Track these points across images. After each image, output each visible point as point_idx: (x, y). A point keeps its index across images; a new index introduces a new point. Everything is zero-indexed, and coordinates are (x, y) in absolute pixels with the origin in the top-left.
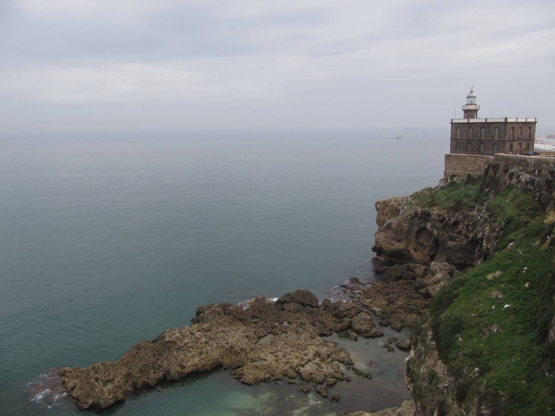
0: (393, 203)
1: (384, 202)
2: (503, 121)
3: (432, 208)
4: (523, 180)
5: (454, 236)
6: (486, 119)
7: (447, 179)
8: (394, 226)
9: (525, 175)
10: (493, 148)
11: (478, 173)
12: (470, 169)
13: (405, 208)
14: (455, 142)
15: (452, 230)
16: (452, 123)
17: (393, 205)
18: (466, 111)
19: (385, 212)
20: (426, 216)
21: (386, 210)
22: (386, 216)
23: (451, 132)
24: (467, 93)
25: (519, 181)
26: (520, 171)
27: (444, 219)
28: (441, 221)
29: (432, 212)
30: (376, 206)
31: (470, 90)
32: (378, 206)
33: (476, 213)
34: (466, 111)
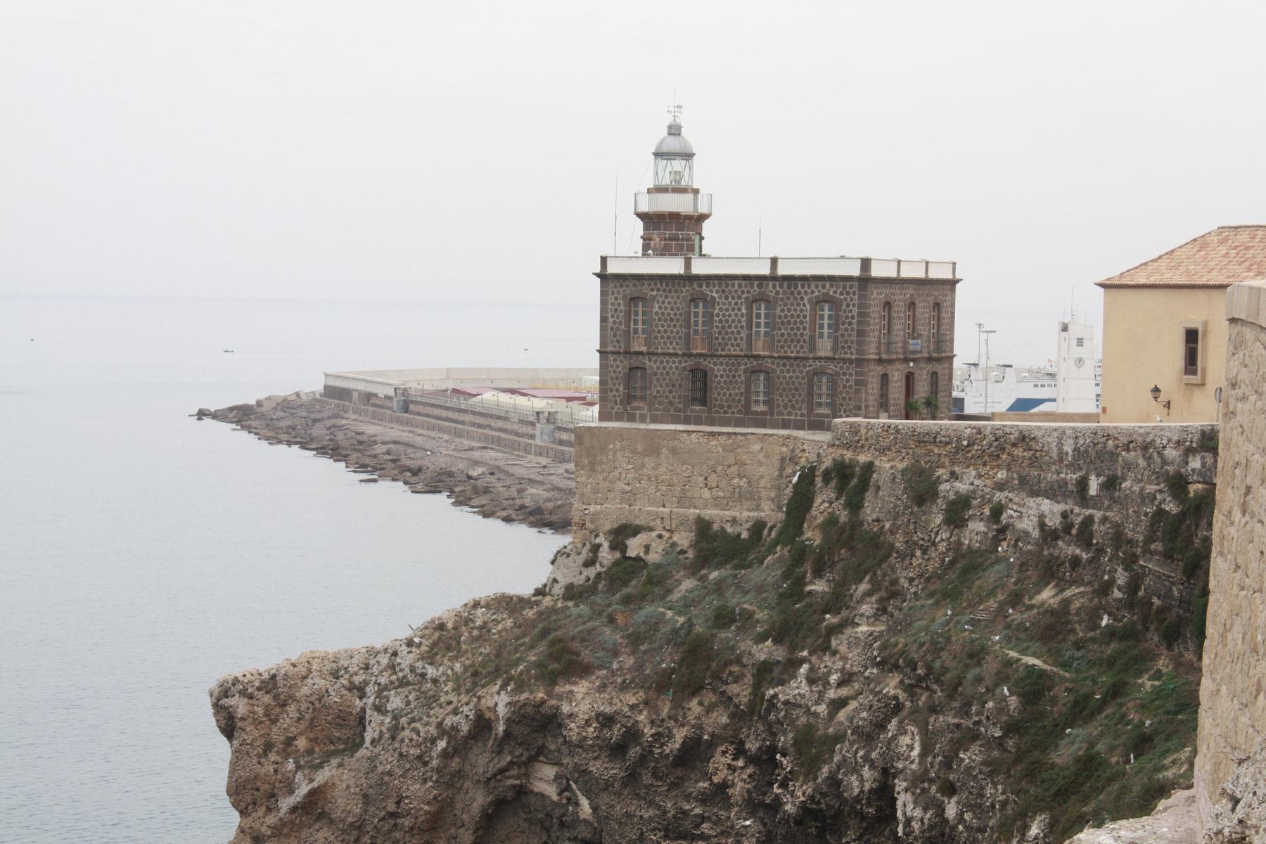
0: (321, 683)
1: (270, 683)
2: (855, 271)
3: (561, 689)
4: (1028, 524)
5: (685, 813)
6: (774, 261)
7: (596, 548)
8: (345, 804)
9: (1031, 502)
10: (810, 394)
11: (746, 515)
12: (706, 494)
13: (395, 702)
14: (621, 365)
15: (674, 785)
16: (603, 276)
17: (322, 695)
18: (651, 220)
19: (277, 735)
20: (536, 728)
21: (285, 722)
22: (285, 753)
23: (603, 319)
24: (657, 135)
25: (1002, 531)
26: (1000, 486)
27: (632, 734)
28: (618, 750)
29: (566, 708)
30: (218, 707)
31: (669, 120)
32: (240, 706)
33: (805, 689)
34: (651, 220)
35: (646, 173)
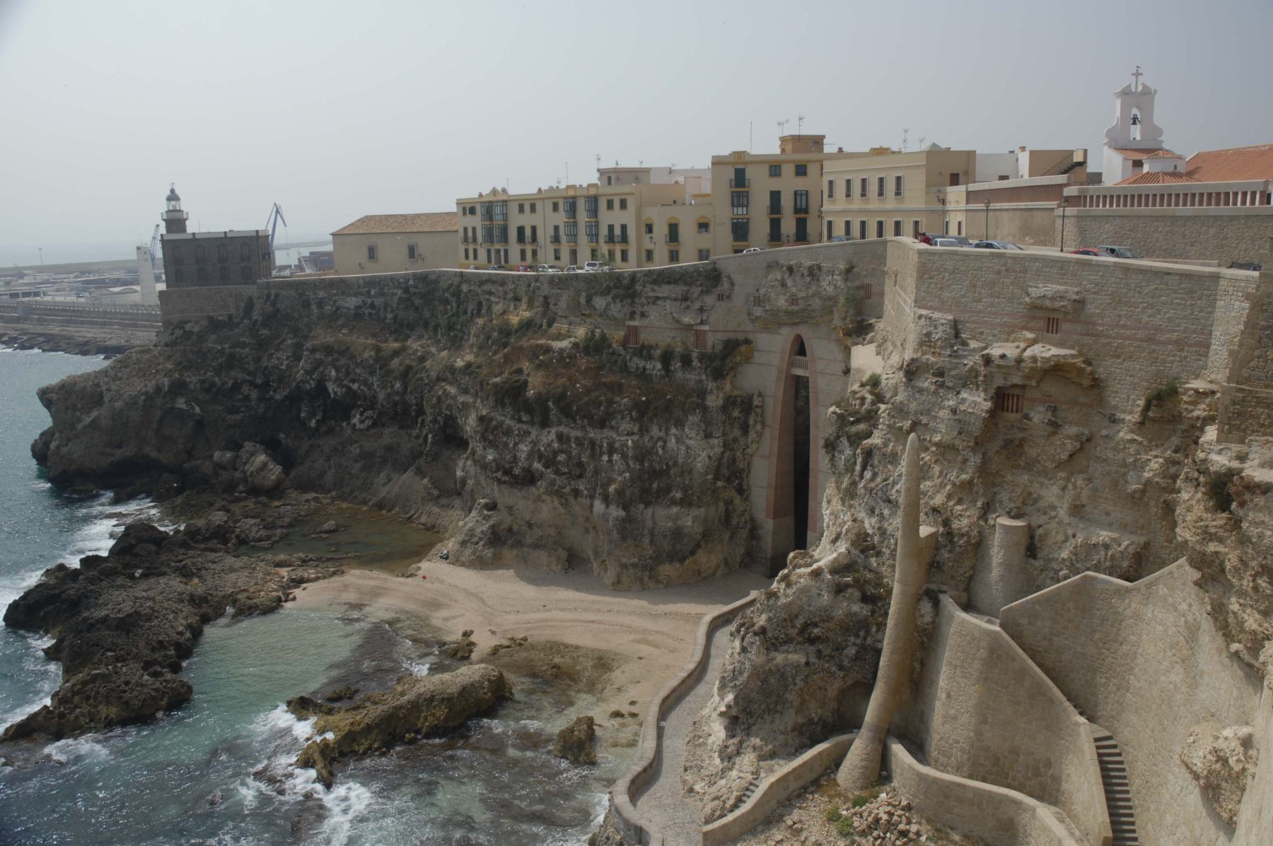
27: (213, 384)
28: (208, 390)
35: (163, 207)
